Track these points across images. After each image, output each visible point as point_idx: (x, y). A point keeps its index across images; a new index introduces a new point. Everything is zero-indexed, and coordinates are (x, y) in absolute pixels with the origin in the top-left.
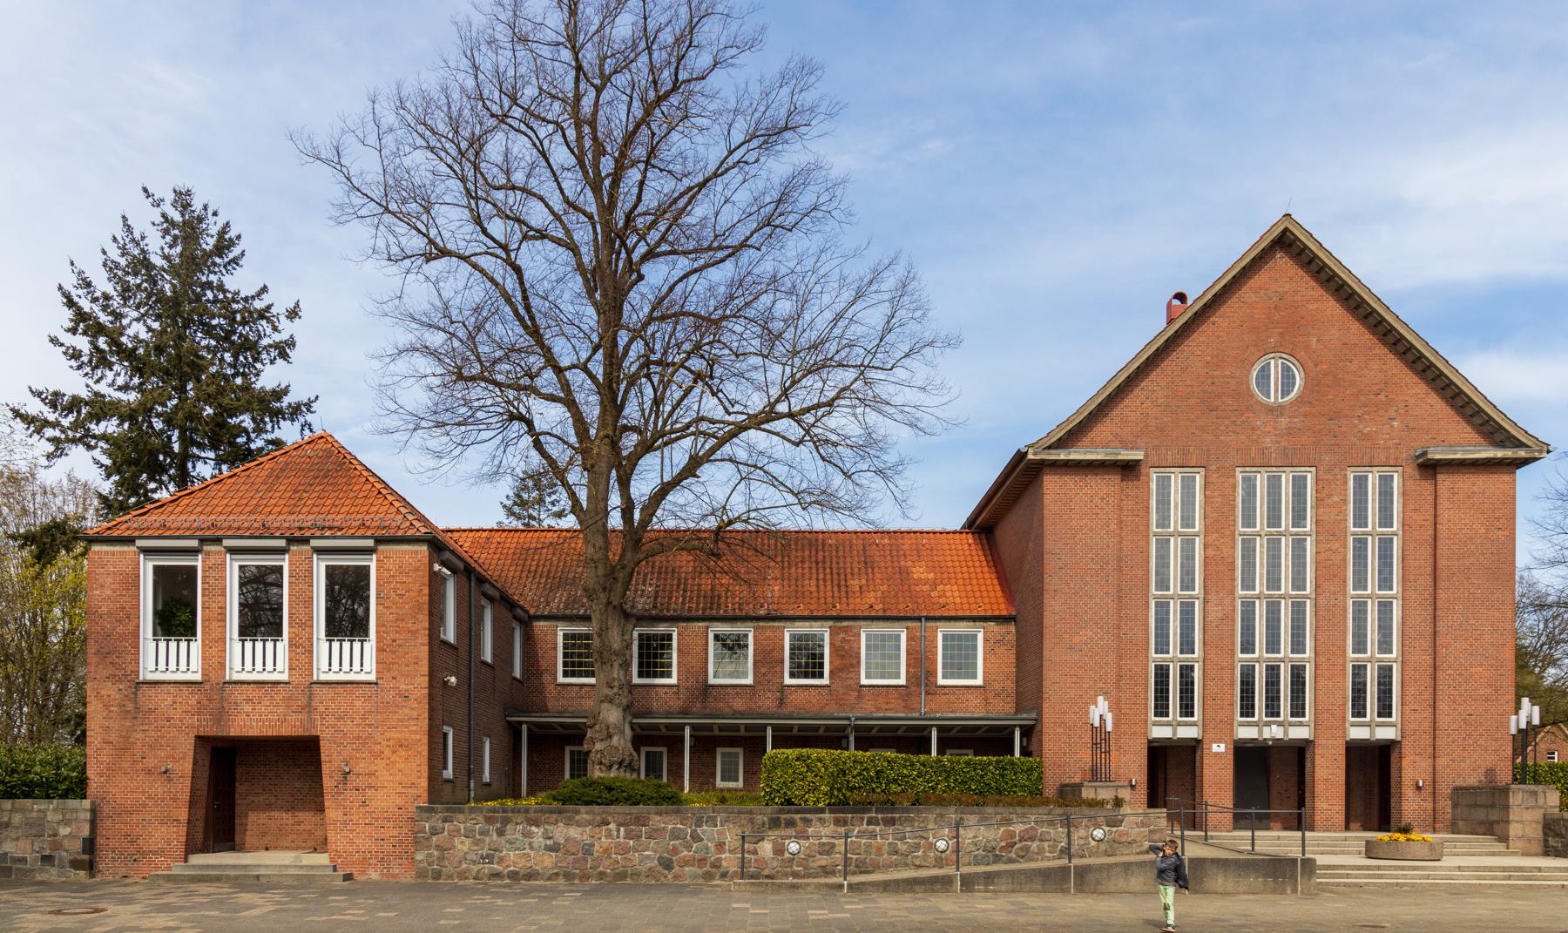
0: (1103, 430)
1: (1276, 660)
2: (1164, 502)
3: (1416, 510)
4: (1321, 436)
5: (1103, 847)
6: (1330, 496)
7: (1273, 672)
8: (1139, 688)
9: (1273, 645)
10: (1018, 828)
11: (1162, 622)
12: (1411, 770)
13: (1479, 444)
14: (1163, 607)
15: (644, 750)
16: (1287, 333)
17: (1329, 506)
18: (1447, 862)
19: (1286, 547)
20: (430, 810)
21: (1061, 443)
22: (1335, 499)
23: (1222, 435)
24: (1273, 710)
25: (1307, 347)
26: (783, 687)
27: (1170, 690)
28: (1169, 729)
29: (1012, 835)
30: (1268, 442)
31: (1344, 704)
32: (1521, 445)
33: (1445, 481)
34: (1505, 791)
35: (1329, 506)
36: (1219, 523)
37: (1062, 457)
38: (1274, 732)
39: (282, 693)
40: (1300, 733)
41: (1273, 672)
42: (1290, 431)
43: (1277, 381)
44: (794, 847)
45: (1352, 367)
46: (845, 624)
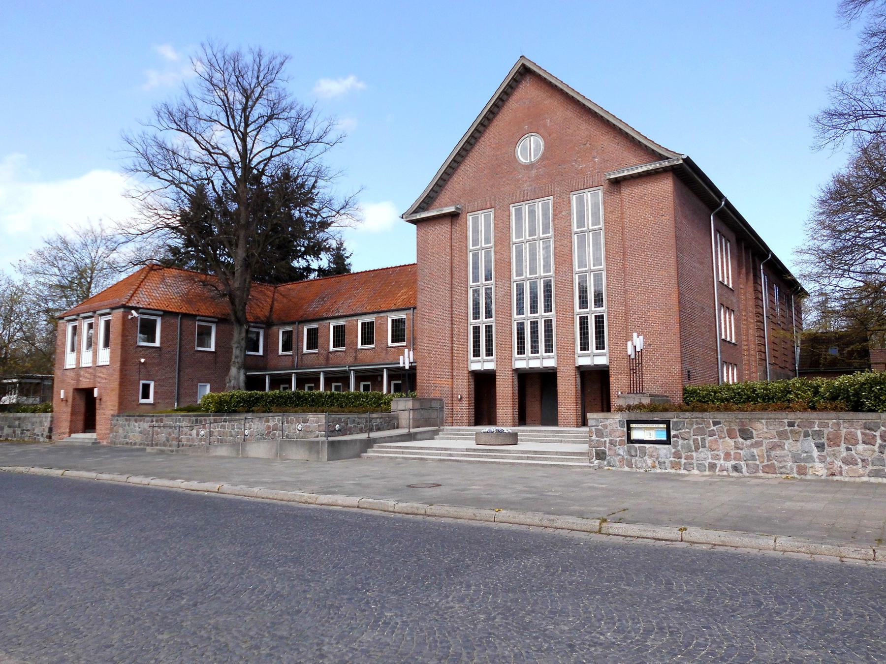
0: (444, 196)
1: (534, 318)
2: (476, 231)
3: (611, 212)
4: (555, 178)
5: (302, 434)
6: (560, 212)
7: (534, 324)
8: (464, 341)
9: (534, 309)
10: (271, 424)
11: (520, 293)
12: (618, 384)
13: (649, 162)
14: (476, 292)
15: (362, 384)
16: (533, 122)
17: (561, 218)
18: (521, 446)
19: (526, 249)
20: (118, 416)
21: (415, 212)
22: (564, 213)
23: (507, 188)
24: (535, 350)
25: (545, 126)
26: (387, 347)
27: (484, 341)
28: (479, 364)
29: (269, 427)
30: (526, 187)
31: (574, 343)
32: (661, 157)
33: (627, 192)
34: (421, 400)
35: (561, 218)
36: (503, 239)
37: (418, 217)
38: (535, 364)
39: (106, 369)
40: (550, 363)
41: (534, 324)
42: (537, 177)
43: (530, 149)
44: (202, 433)
45: (570, 131)
46: (382, 315)
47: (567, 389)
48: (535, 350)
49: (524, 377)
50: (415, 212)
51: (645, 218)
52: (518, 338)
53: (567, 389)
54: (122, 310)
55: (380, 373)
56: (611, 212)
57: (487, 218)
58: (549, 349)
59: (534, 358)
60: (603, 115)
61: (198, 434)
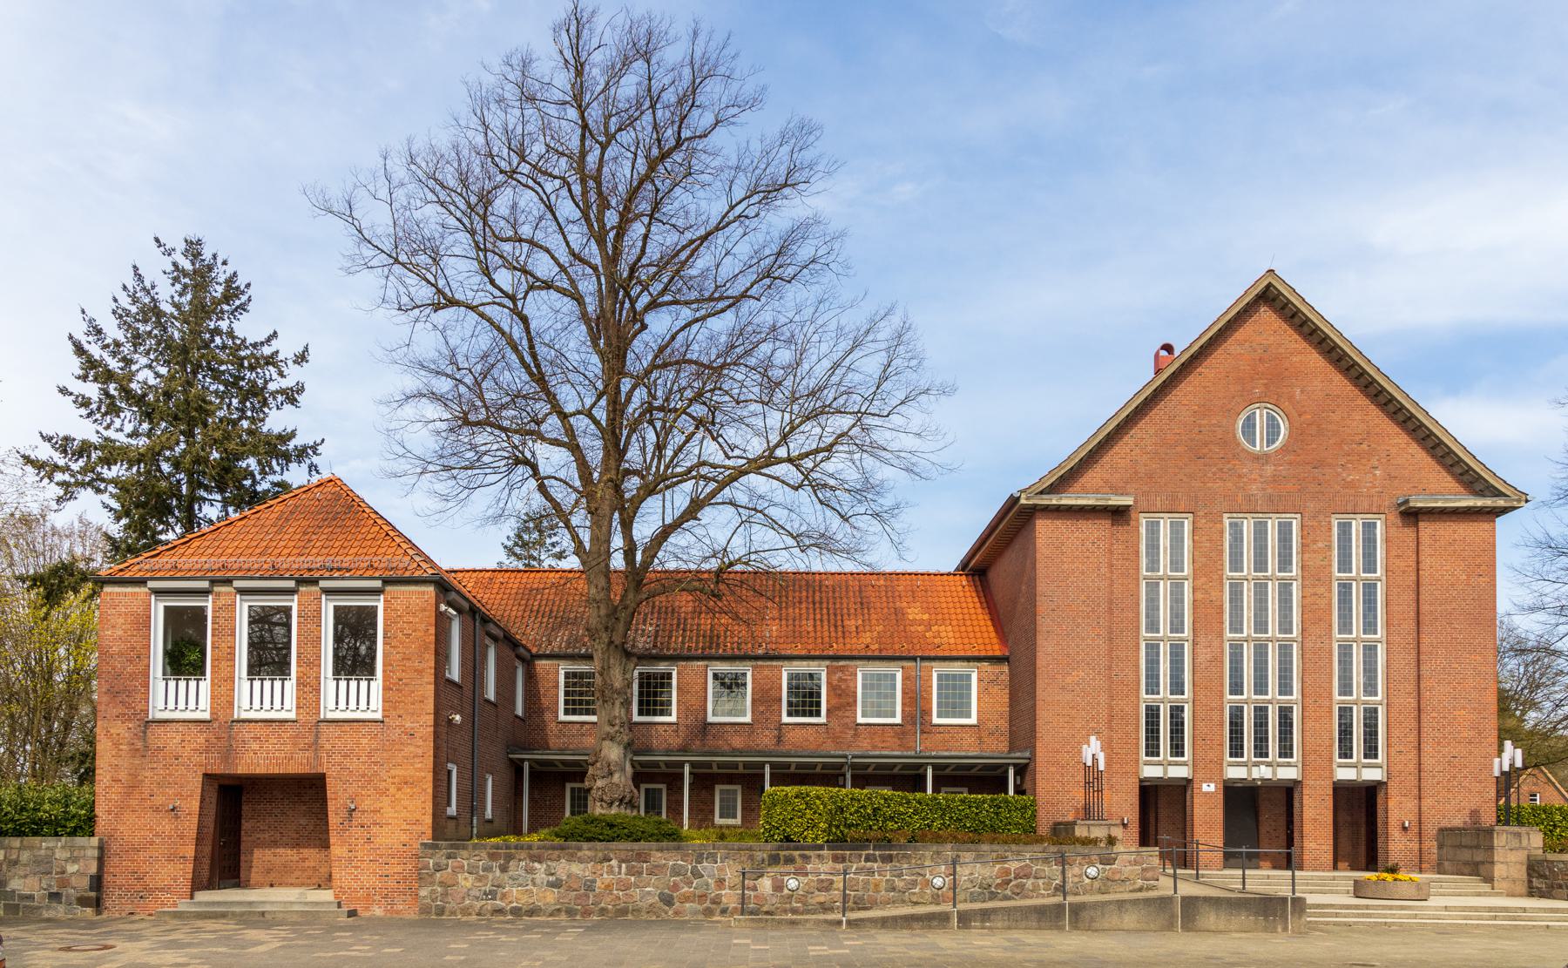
0: (1093, 476)
1: (1264, 701)
2: (1153, 547)
3: (1398, 556)
4: (1305, 482)
5: (1096, 884)
6: (1315, 542)
7: (1261, 713)
9: (1261, 687)
10: (1013, 866)
11: (1153, 663)
12: (1397, 810)
14: (1153, 649)
16: (1272, 383)
18: (1434, 902)
19: (1164, 589)
20: (434, 847)
22: (1320, 545)
24: (1261, 750)
25: (1291, 398)
29: (1007, 872)
30: (1254, 489)
32: (1498, 494)
33: (1427, 528)
38: (1262, 772)
40: (1288, 774)
41: (1261, 713)
42: (1275, 479)
43: (1263, 430)
44: (793, 884)
45: (1335, 417)
47: (1316, 815)
48: (1261, 750)
49: (1344, 793)
50: (1053, 489)
51: (1453, 575)
52: (1231, 732)
53: (1316, 815)
54: (431, 589)
55: (678, 770)
56: (1398, 556)
57: (1176, 529)
58: (1286, 751)
59: (1177, 764)
60: (1142, 398)
61: (778, 887)
